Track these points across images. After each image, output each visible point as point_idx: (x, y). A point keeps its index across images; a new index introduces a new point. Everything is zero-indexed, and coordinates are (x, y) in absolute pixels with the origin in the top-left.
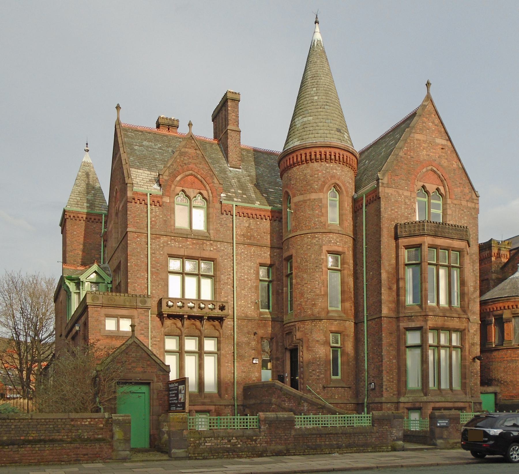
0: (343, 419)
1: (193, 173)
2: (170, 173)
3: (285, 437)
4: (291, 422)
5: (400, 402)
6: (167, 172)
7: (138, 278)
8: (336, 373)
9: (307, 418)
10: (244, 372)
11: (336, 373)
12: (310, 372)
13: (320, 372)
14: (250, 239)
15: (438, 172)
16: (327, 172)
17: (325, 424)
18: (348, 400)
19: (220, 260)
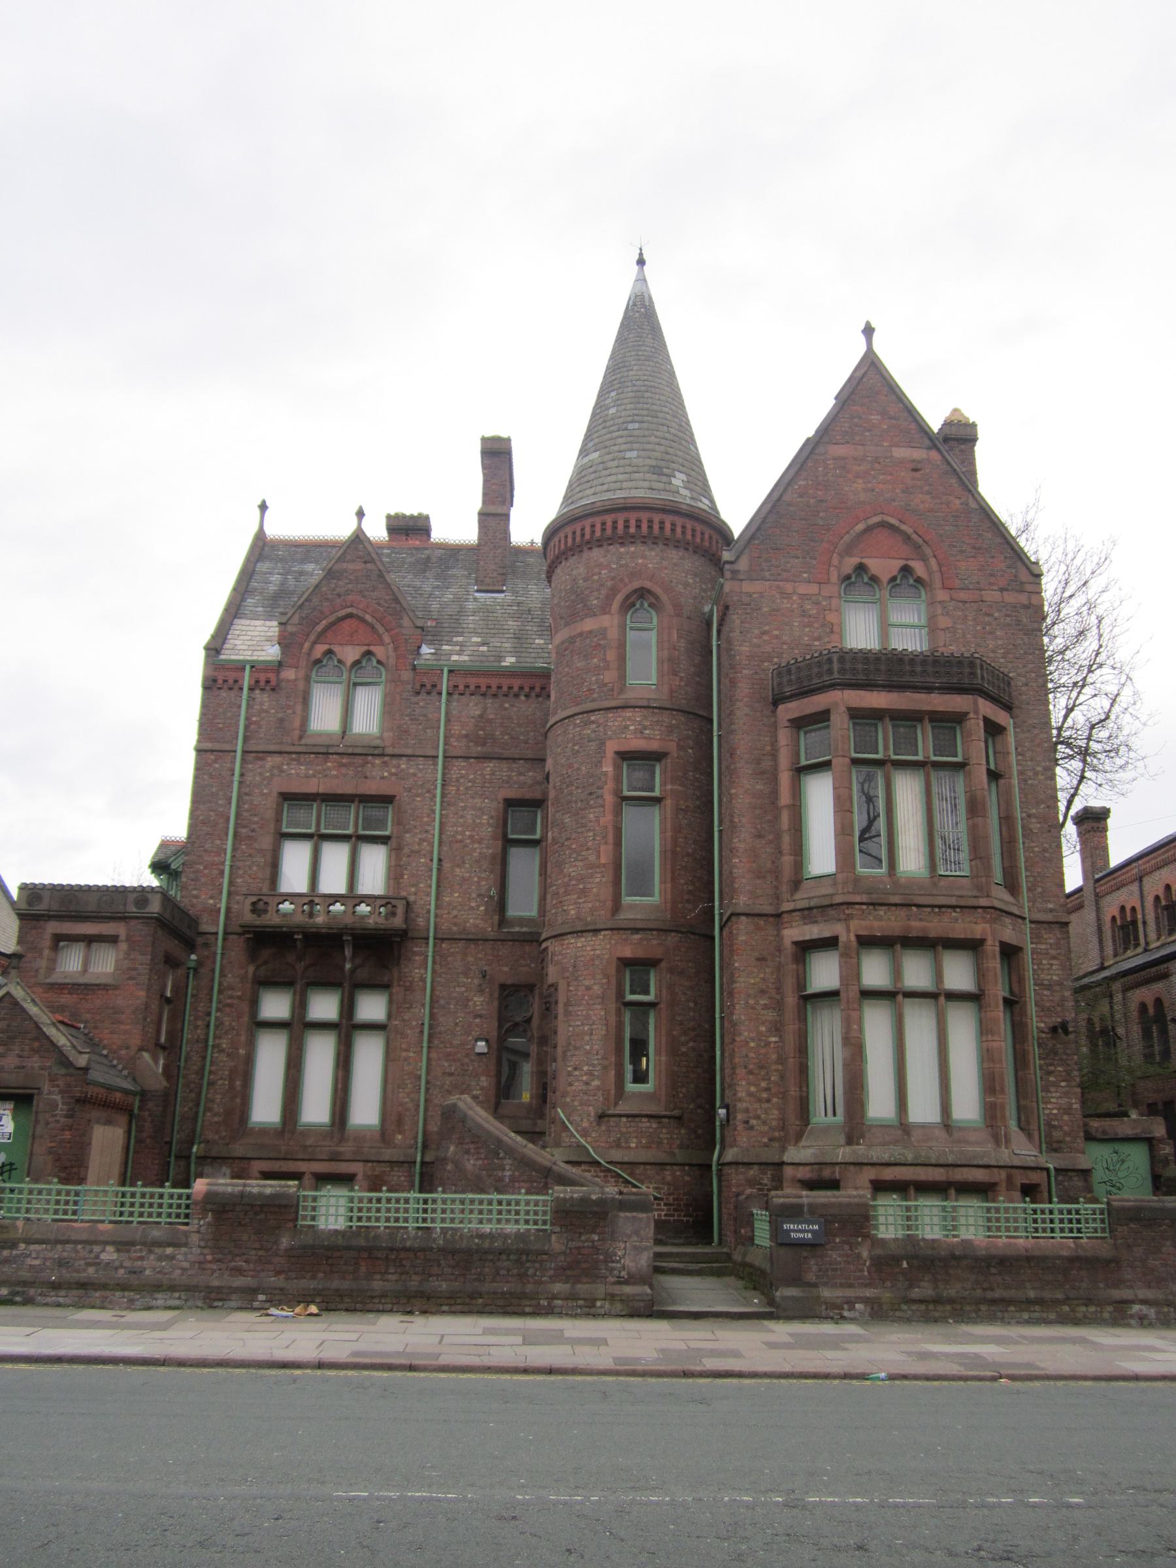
0: (1047, 1216)
1: (354, 611)
2: (302, 618)
3: (261, 1253)
4: (282, 1212)
5: (783, 1163)
6: (297, 617)
7: (206, 851)
9: (509, 1204)
10: (451, 1074)
11: (640, 1077)
12: (570, 1074)
13: (590, 1073)
14: (484, 744)
15: (903, 527)
16: (621, 566)
17: (397, 1220)
18: (673, 1154)
19: (404, 797)
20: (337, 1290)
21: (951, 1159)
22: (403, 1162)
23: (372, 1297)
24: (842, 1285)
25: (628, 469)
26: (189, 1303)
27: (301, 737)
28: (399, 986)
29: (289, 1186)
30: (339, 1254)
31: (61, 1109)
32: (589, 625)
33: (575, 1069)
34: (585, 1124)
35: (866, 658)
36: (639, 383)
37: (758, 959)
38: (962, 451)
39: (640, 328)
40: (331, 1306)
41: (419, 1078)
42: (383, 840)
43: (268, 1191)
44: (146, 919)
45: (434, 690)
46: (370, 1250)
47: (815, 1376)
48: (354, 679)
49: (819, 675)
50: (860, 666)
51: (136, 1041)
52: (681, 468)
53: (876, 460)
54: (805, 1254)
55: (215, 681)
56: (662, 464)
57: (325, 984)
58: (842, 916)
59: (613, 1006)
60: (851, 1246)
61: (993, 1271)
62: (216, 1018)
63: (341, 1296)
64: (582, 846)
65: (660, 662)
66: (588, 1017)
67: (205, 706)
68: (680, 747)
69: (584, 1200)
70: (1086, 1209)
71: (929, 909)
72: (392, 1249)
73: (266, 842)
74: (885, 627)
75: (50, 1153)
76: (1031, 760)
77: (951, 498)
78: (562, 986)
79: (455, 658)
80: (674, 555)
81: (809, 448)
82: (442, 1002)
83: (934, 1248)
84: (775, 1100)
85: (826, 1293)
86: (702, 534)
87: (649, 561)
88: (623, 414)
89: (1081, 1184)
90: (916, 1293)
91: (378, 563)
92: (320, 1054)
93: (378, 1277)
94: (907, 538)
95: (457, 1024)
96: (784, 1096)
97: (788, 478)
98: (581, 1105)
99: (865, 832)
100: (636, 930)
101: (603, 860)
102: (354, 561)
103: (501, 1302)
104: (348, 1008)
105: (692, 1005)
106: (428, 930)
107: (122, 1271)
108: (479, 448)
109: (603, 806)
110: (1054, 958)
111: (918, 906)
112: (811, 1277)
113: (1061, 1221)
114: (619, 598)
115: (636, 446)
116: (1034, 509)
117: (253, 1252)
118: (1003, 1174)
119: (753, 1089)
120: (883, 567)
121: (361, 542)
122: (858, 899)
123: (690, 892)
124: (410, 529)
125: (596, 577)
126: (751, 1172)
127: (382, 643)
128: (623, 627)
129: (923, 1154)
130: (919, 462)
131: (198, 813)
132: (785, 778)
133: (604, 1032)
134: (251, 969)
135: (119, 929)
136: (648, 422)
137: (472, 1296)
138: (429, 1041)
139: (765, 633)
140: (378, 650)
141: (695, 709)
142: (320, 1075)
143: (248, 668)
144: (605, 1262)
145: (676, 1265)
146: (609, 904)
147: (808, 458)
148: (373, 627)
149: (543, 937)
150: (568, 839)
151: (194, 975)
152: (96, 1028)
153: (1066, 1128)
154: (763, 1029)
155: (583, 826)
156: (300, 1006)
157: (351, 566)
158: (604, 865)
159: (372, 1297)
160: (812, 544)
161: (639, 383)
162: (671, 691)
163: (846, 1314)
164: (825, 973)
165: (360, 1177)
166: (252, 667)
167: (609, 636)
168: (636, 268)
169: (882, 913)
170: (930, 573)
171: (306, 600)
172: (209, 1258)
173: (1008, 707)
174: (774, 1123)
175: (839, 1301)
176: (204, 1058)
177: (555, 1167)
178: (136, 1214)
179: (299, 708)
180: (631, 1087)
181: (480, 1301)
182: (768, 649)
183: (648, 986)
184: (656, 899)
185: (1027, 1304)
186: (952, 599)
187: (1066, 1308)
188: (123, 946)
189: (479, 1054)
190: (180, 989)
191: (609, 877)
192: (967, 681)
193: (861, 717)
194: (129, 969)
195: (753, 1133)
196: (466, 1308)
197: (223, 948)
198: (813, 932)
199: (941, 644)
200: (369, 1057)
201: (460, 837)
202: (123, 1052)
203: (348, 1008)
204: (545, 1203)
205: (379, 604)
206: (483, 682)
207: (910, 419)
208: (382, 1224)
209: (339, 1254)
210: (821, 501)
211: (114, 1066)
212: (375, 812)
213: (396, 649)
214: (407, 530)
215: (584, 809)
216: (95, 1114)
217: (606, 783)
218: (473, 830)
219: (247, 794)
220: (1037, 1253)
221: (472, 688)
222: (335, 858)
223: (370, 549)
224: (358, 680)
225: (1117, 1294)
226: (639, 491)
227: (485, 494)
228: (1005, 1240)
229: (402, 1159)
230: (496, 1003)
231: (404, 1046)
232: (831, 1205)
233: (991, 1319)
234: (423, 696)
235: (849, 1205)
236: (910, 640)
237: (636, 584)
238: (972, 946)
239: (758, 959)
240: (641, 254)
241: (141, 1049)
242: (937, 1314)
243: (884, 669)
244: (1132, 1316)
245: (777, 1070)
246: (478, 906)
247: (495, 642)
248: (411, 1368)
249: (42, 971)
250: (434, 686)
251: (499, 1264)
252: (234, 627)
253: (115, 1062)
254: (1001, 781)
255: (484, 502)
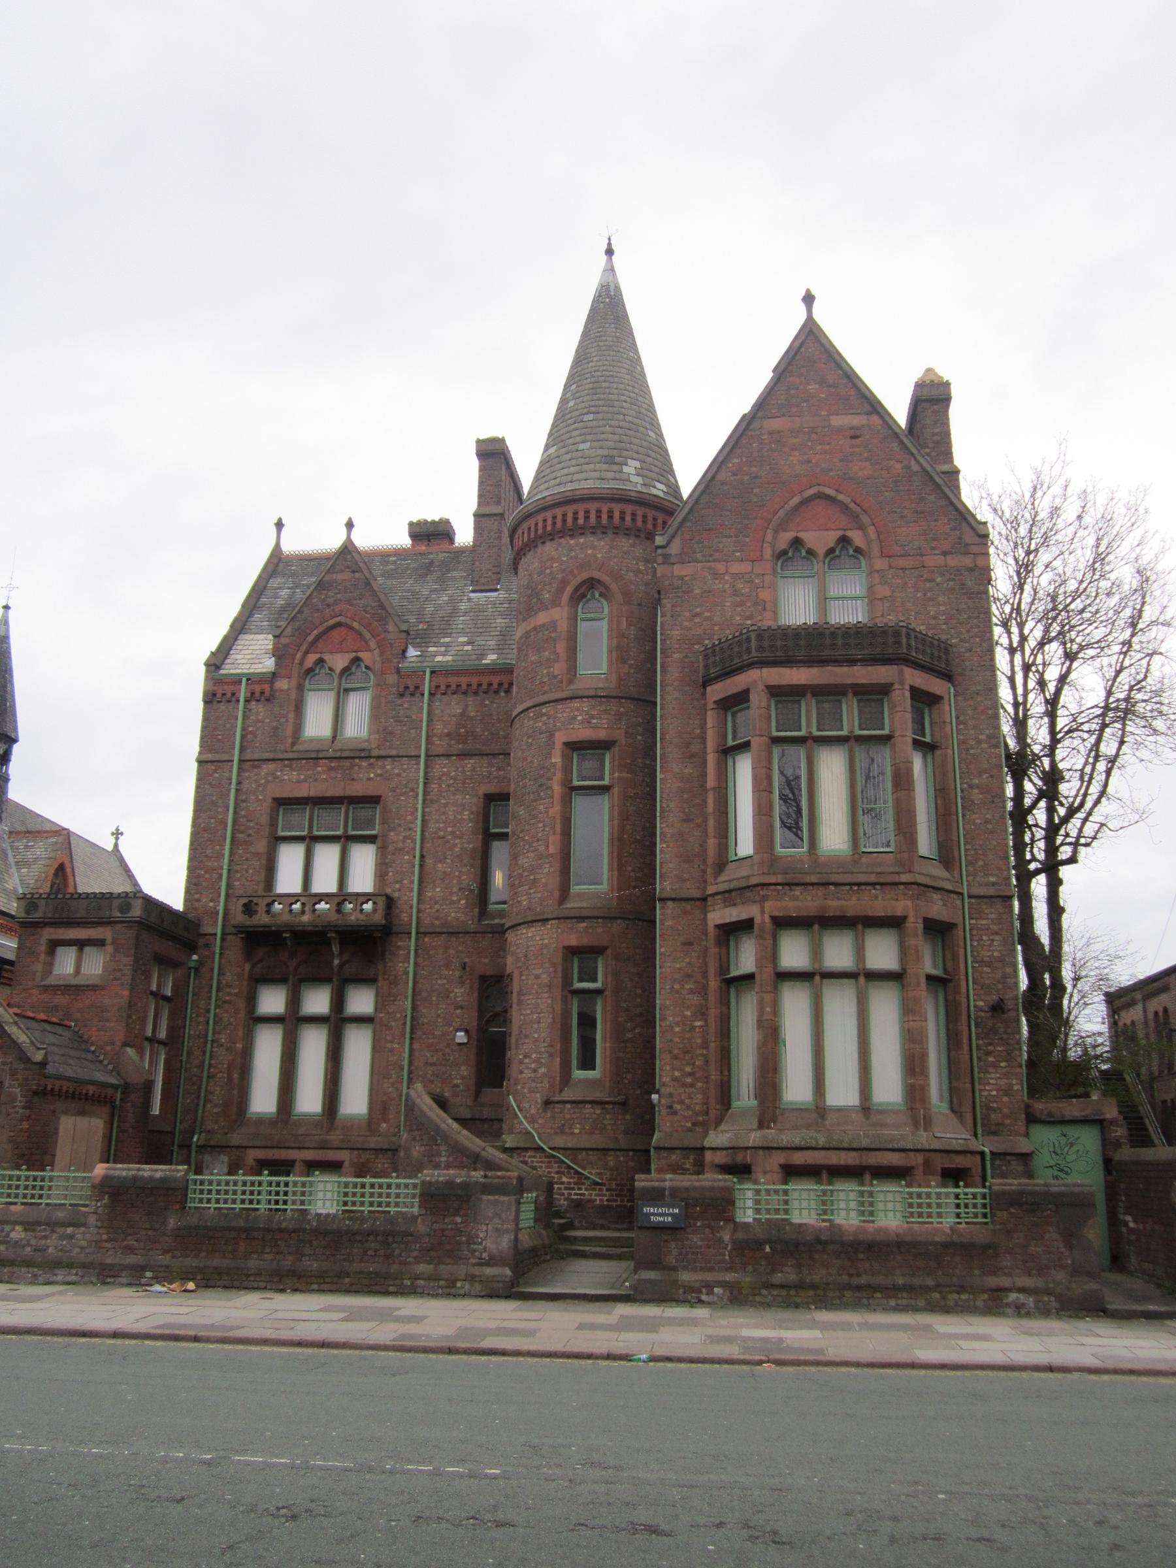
3: (150, 1233)
4: (175, 1193)
5: (702, 1149)
8: (587, 1062)
10: (432, 1064)
11: (587, 1062)
13: (537, 1061)
14: (464, 742)
15: (841, 497)
16: (571, 558)
18: (617, 1140)
20: (216, 1268)
21: (865, 1143)
22: (387, 1150)
23: (249, 1275)
24: (702, 1269)
25: (581, 461)
26: (85, 1279)
27: (293, 744)
28: (385, 980)
29: (178, 1171)
30: (220, 1234)
31: (20, 1101)
32: (542, 618)
33: (525, 1057)
34: (533, 1111)
35: (785, 635)
36: (606, 371)
37: (684, 944)
38: (934, 412)
39: (608, 319)
40: (211, 1283)
41: (402, 1068)
42: (371, 839)
43: (158, 1175)
44: (130, 923)
45: (417, 690)
46: (247, 1230)
47: (692, 1360)
48: (344, 685)
49: (740, 654)
50: (779, 643)
51: (120, 1037)
52: (635, 455)
53: (813, 430)
54: (665, 1238)
55: (214, 695)
56: (615, 452)
57: (318, 980)
58: (757, 898)
59: (558, 994)
60: (712, 1228)
61: (861, 1256)
62: (216, 1015)
63: (220, 1274)
64: (533, 837)
65: (610, 651)
66: (536, 1006)
67: (206, 719)
68: (628, 735)
69: (449, 1184)
70: (966, 1194)
71: (848, 887)
72: (269, 1230)
73: (261, 846)
74: (823, 601)
75: (10, 1142)
76: (974, 728)
77: (892, 462)
78: (516, 976)
79: (439, 659)
80: (624, 543)
81: (744, 424)
82: (425, 994)
83: (799, 1233)
84: (699, 1084)
85: (685, 1277)
86: (655, 519)
87: (596, 551)
88: (580, 406)
89: (1020, 1168)
90: (778, 1278)
91: (366, 572)
92: (313, 1047)
93: (255, 1256)
94: (845, 508)
95: (438, 1016)
96: (706, 1079)
97: (721, 458)
98: (530, 1092)
99: (791, 807)
100: (581, 919)
101: (551, 851)
102: (342, 571)
103: (365, 1282)
104: (338, 1002)
105: (639, 991)
106: (411, 924)
107: (28, 1249)
108: (474, 451)
109: (552, 797)
110: (996, 933)
111: (836, 884)
112: (671, 1260)
113: (218, 1192)
114: (569, 589)
115: (589, 437)
116: (1060, 464)
117: (144, 1232)
118: (920, 1158)
119: (677, 1074)
120: (819, 539)
121: (350, 552)
122: (773, 879)
123: (637, 879)
124: (432, 534)
125: (548, 571)
126: (674, 1157)
127: (369, 650)
128: (573, 621)
129: (836, 1137)
130: (858, 428)
131: (200, 820)
132: (711, 759)
133: (550, 1020)
134: (247, 967)
135: (105, 933)
136: (604, 412)
137: (340, 1275)
138: (412, 1032)
139: (696, 615)
140: (365, 656)
141: (637, 696)
142: (310, 1066)
143: (244, 680)
144: (468, 1244)
145: (598, 1249)
146: (557, 893)
147: (741, 435)
148: (360, 634)
149: (507, 926)
150: (522, 831)
151: (195, 974)
152: (85, 1026)
153: (1006, 1110)
154: (688, 1013)
155: (535, 817)
156: (294, 1001)
157: (340, 577)
158: (552, 856)
159: (249, 1275)
160: (746, 522)
161: (606, 371)
162: (620, 679)
163: (704, 1297)
164: (746, 958)
165: (346, 1164)
166: (248, 680)
167: (559, 629)
168: (605, 257)
169: (798, 893)
170: (869, 542)
171: (299, 612)
172: (105, 1237)
173: (948, 677)
174: (698, 1108)
175: (697, 1285)
176: (204, 1053)
177: (483, 1153)
178: (213, 1201)
179: (291, 716)
180: (578, 1074)
181: (347, 1280)
182: (699, 631)
183: (596, 974)
184: (604, 887)
185: (892, 1291)
186: (891, 567)
187: (937, 1296)
188: (110, 949)
189: (460, 1044)
190: (180, 989)
191: (557, 866)
192: (890, 651)
193: (782, 694)
194: (115, 970)
195: (676, 1118)
196: (333, 1287)
197: (222, 948)
198: (733, 914)
199: (879, 614)
200: (359, 1049)
201: (442, 833)
202: (109, 1048)
203: (338, 1002)
204: (415, 1186)
205: (366, 611)
206: (464, 680)
207: (850, 385)
208: (213, 1205)
209: (220, 1234)
210: (756, 477)
211: (101, 1062)
212: (364, 813)
213: (381, 654)
214: (428, 536)
215: (535, 801)
216: (59, 1105)
217: (554, 774)
218: (454, 826)
219: (244, 801)
220: (908, 1239)
221: (454, 687)
222: (327, 858)
223: (357, 557)
224: (313, 687)
225: (992, 1281)
226: (588, 483)
227: (480, 496)
228: (19, 1208)
229: (385, 1147)
230: (476, 995)
231: (388, 1038)
232: (694, 1188)
233: (855, 1305)
234: (407, 698)
235: (712, 1189)
236: (849, 611)
237: (585, 575)
238: (894, 923)
239: (684, 944)
240: (609, 244)
241: (125, 1045)
242: (799, 1300)
243: (815, 644)
244: (1008, 1305)
245: (702, 1055)
246: (459, 900)
247: (480, 641)
248: (196, 1339)
249: (39, 974)
250: (417, 687)
251: (367, 1245)
252: (238, 642)
253: (102, 1058)
254: (938, 752)
255: (479, 504)
